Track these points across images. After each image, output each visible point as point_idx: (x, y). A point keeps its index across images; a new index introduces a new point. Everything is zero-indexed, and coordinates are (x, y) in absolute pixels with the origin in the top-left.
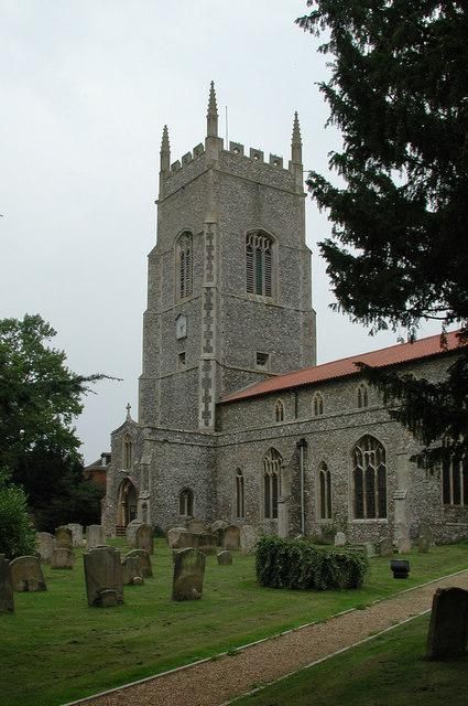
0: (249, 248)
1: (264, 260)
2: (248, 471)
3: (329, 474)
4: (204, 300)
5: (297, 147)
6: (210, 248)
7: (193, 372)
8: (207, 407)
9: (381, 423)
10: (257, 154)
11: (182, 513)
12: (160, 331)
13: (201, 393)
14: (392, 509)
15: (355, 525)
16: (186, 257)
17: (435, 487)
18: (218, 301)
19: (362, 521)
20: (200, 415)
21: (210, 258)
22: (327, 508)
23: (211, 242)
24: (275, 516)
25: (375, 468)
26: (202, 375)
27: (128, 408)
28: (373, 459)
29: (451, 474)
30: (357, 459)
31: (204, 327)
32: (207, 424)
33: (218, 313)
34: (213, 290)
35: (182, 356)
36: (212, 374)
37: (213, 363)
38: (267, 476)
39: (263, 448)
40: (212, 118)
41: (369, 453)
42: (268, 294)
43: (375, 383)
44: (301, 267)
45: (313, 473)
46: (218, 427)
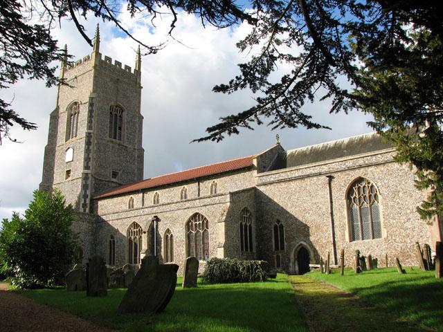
0: (111, 113)
1: (118, 120)
3: (114, 241)
8: (85, 201)
9: (205, 206)
10: (118, 63)
20: (81, 205)
32: (85, 211)
34: (92, 135)
35: (68, 172)
41: (198, 223)
42: (120, 139)
44: (137, 125)
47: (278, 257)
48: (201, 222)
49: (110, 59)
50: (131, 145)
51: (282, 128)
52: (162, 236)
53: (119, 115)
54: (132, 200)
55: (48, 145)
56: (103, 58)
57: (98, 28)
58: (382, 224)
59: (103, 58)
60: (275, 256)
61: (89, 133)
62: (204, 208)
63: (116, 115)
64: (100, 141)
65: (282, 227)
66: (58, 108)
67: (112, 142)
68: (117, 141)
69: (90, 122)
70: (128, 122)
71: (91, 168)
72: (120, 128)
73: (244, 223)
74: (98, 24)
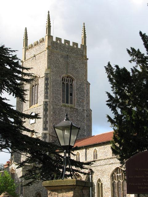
0: (63, 83)
5: (99, 160)
18: (50, 107)
23: (47, 82)
34: (48, 103)
41: (119, 175)
42: (71, 103)
43: (114, 154)
44: (85, 90)
48: (121, 174)
49: (60, 39)
50: (80, 108)
52: (95, 184)
53: (69, 84)
54: (95, 152)
56: (54, 40)
57: (49, 15)
59: (54, 40)
61: (46, 102)
64: (55, 107)
66: (7, 100)
67: (65, 106)
68: (69, 105)
69: (46, 93)
70: (77, 89)
71: (48, 129)
72: (71, 95)
74: (49, 12)
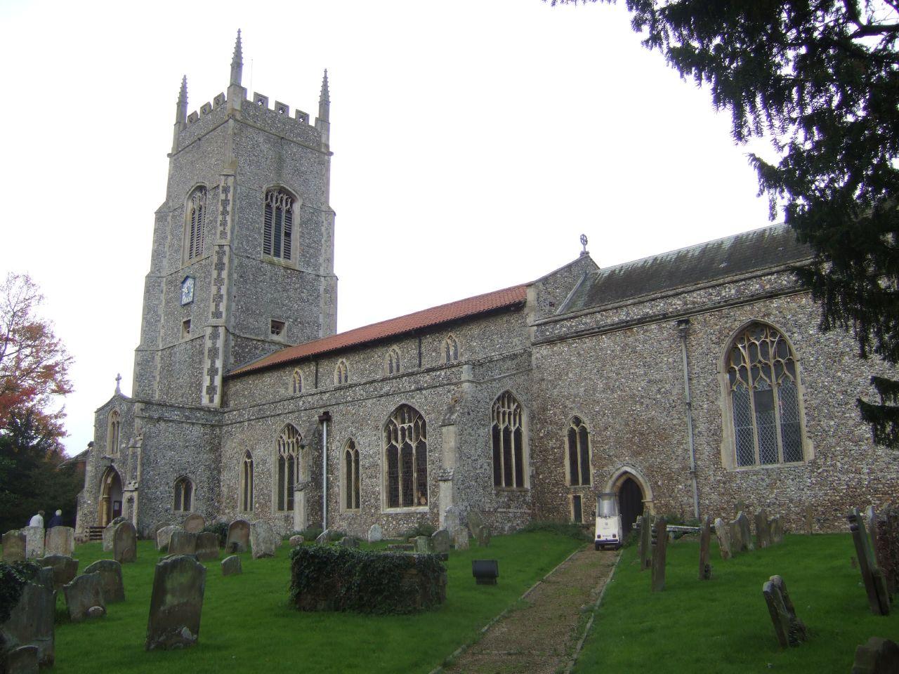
0: (268, 206)
2: (258, 454)
3: (357, 453)
4: (215, 259)
5: (324, 103)
6: (225, 202)
7: (198, 342)
8: (212, 381)
9: (420, 389)
10: (282, 107)
11: (177, 507)
12: (163, 297)
13: (207, 364)
14: (434, 494)
15: (388, 515)
16: (198, 213)
17: (485, 466)
18: (231, 261)
19: (398, 510)
21: (225, 213)
22: (354, 497)
23: (227, 196)
24: (291, 507)
25: (414, 445)
26: (208, 344)
27: (118, 379)
28: (410, 433)
29: (502, 450)
30: (391, 434)
31: (214, 290)
32: (211, 400)
33: (230, 275)
34: (227, 249)
35: (187, 323)
36: (220, 343)
37: (221, 331)
38: (281, 460)
39: (278, 425)
40: (237, 66)
41: (406, 426)
42: (287, 256)
45: (339, 456)
46: (224, 403)
47: (577, 498)
48: (412, 425)
51: (194, 212)
53: (284, 208)
55: (152, 272)
58: (804, 429)
60: (570, 496)
62: (417, 395)
63: (278, 208)
64: (246, 261)
65: (584, 433)
68: (282, 260)
72: (288, 235)
73: (502, 427)
